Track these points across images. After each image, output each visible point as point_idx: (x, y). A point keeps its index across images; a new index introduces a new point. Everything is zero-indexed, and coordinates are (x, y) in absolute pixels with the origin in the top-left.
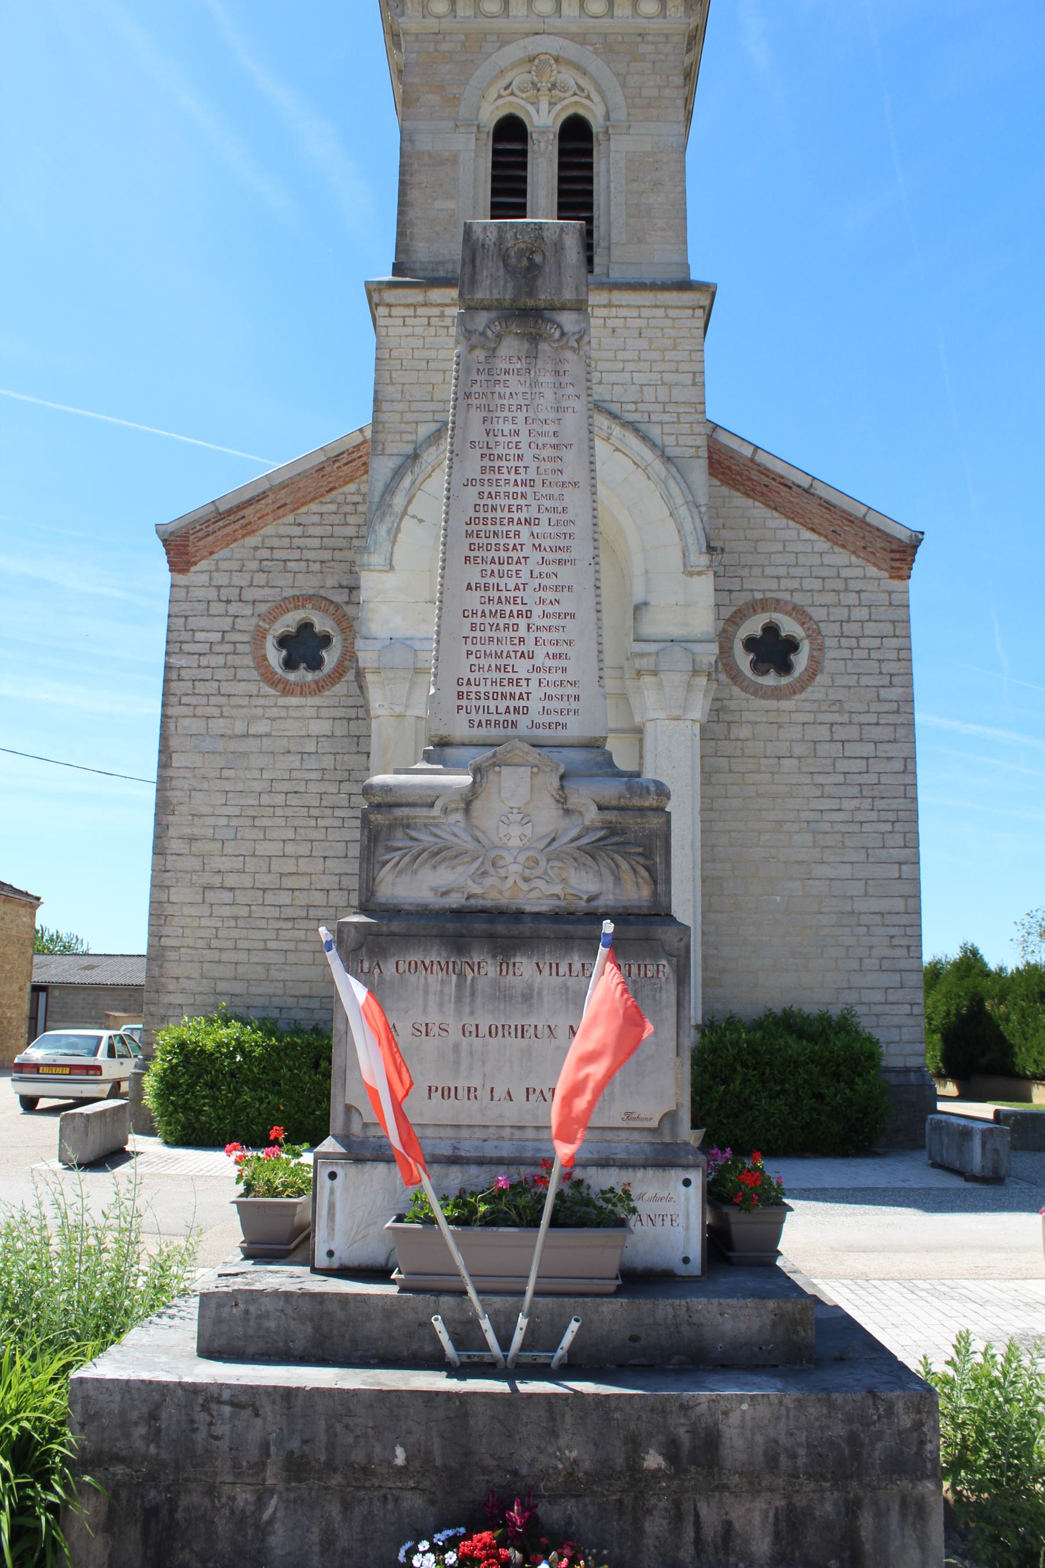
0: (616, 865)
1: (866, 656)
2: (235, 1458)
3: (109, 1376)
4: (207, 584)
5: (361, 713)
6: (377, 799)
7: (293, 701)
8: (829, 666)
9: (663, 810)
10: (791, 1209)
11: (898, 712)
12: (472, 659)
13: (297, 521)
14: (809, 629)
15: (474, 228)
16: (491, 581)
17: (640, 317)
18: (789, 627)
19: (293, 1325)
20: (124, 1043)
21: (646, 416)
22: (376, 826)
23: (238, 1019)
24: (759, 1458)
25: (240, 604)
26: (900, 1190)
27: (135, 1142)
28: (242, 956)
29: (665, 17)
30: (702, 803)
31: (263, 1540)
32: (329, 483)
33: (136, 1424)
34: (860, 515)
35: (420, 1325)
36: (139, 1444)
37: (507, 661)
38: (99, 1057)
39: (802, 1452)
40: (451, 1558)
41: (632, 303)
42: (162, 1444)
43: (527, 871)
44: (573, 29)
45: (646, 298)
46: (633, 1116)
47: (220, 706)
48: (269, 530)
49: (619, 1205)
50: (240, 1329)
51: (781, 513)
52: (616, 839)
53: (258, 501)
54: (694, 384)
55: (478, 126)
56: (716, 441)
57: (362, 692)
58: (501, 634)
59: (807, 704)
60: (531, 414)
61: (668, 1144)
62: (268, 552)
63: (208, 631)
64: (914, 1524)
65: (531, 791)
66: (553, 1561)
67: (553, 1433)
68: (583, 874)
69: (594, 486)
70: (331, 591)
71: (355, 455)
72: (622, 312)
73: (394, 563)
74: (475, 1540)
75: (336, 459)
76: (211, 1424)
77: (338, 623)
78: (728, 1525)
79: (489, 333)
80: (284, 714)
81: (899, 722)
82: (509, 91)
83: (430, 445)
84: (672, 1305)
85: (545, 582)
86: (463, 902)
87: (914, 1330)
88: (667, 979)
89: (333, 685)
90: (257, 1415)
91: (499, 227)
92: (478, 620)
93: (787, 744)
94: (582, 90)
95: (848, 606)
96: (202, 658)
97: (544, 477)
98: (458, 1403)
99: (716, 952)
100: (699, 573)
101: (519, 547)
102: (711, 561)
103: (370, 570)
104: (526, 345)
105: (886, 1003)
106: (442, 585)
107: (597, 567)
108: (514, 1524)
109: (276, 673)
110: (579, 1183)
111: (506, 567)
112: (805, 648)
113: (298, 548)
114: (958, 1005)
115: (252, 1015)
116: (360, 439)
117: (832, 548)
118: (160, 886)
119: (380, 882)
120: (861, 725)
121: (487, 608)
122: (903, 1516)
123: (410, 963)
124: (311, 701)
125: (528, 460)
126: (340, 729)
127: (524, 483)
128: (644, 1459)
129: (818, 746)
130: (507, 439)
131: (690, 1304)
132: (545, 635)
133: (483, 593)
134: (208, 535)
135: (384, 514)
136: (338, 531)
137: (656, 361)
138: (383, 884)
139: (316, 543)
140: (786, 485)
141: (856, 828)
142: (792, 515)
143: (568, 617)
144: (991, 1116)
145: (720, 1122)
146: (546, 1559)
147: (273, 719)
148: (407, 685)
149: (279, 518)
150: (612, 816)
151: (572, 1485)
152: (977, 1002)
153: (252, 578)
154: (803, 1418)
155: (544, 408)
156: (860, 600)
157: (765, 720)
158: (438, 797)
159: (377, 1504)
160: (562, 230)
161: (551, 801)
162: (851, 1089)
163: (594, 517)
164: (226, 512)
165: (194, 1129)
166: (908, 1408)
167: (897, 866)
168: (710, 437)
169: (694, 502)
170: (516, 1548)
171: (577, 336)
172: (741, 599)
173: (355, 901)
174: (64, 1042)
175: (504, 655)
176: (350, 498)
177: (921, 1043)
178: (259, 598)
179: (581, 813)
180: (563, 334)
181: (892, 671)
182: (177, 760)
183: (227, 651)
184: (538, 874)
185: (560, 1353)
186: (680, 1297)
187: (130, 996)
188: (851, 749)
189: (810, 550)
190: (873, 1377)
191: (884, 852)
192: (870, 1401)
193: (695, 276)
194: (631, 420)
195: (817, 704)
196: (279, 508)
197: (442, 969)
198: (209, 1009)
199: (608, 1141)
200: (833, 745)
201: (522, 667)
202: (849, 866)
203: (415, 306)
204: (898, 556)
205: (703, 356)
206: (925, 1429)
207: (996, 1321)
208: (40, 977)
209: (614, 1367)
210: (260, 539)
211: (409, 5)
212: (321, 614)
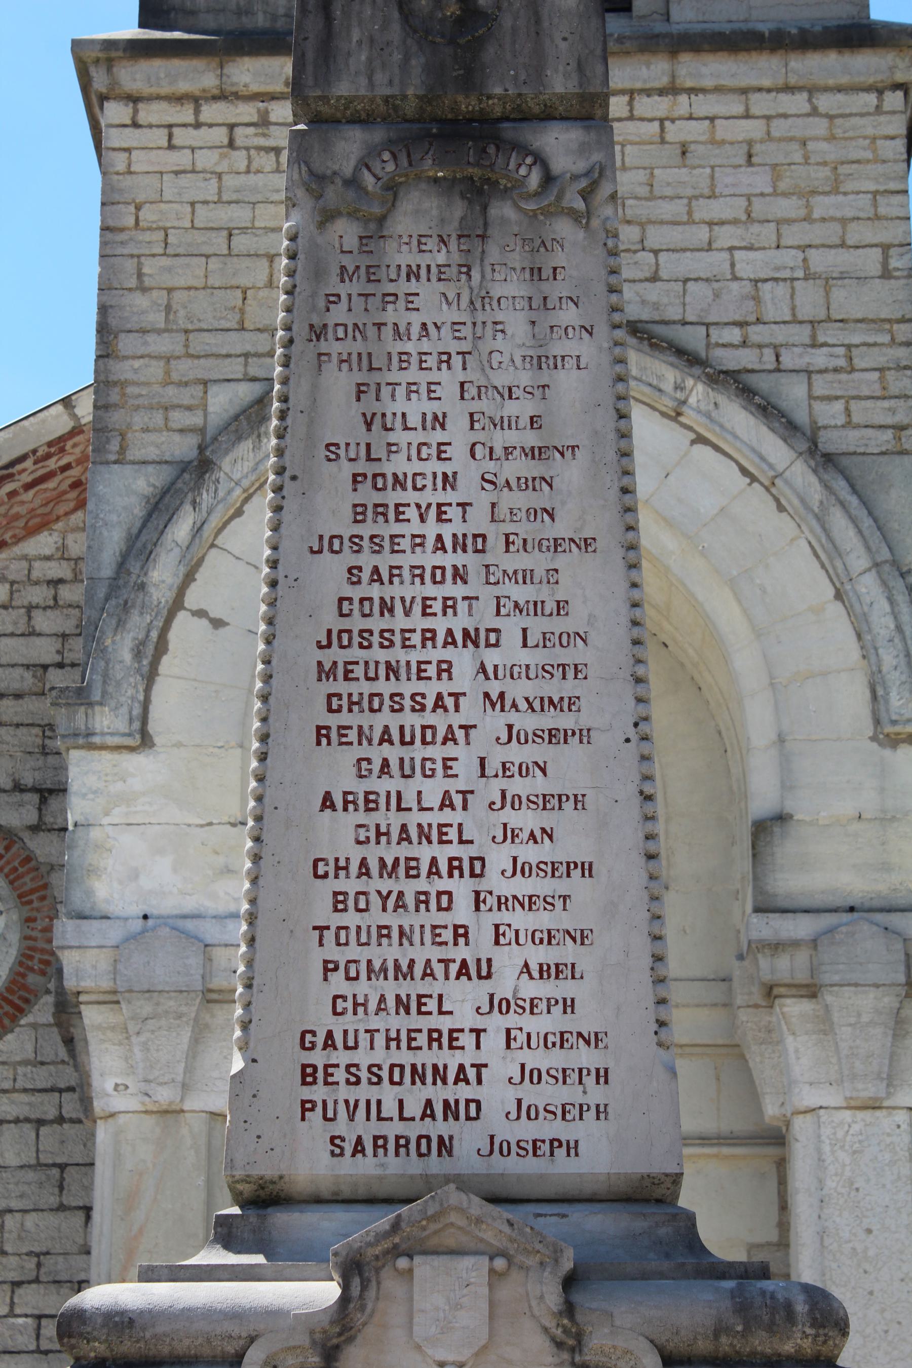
5: (70, 1108)
17: (747, 116)
37: (422, 987)
45: (762, 68)
58: (409, 919)
60: (473, 375)
65: (492, 1316)
72: (704, 105)
73: (151, 728)
79: (369, 180)
83: (239, 439)
85: (517, 786)
92: (351, 885)
97: (509, 528)
103: (92, 747)
104: (459, 209)
107: (646, 748)
111: (418, 752)
116: (64, 424)
127: (460, 544)
130: (416, 437)
132: (520, 919)
133: (361, 817)
135: (126, 607)
137: (789, 221)
148: (186, 1035)
155: (506, 359)
158: (252, 1340)
161: (539, 1344)
169: (895, 563)
171: (583, 183)
175: (418, 970)
176: (42, 570)
180: (548, 179)
194: (732, 366)
201: (464, 1001)
203: (196, 100)
205: (905, 206)
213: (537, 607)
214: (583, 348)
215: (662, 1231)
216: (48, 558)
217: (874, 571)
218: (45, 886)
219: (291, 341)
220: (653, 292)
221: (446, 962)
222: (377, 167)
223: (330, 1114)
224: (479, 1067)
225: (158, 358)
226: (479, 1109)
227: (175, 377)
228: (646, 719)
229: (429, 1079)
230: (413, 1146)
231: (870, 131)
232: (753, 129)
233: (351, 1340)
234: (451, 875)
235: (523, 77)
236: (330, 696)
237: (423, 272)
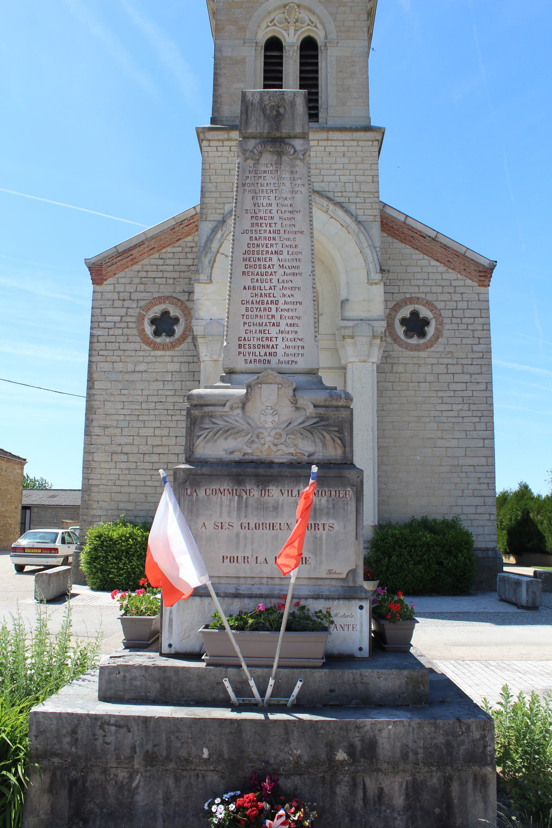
0: (323, 436)
1: (466, 328)
2: (118, 754)
3: (50, 711)
4: (112, 291)
5: (195, 359)
6: (195, 402)
7: (159, 353)
8: (446, 333)
9: (349, 407)
10: (418, 622)
11: (483, 358)
12: (246, 327)
14: (435, 313)
15: (247, 94)
16: (257, 284)
17: (344, 146)
18: (424, 312)
19: (149, 684)
20: (70, 536)
21: (347, 199)
22: (195, 417)
23: (131, 523)
24: (398, 754)
27: (75, 589)
28: (132, 490)
31: (133, 798)
33: (65, 736)
36: (66, 747)
38: (56, 543)
39: (421, 751)
40: (232, 807)
41: (339, 138)
42: (79, 747)
45: (347, 135)
46: (332, 572)
47: (120, 356)
48: (145, 262)
49: (325, 619)
51: (420, 251)
52: (323, 423)
53: (140, 246)
54: (373, 182)
55: (256, 43)
57: (196, 348)
58: (262, 313)
59: (434, 354)
60: (278, 195)
62: (145, 273)
63: (113, 316)
64: (480, 789)
65: (278, 397)
66: (287, 809)
67: (287, 741)
69: (312, 233)
70: (179, 294)
71: (191, 221)
72: (334, 143)
73: (212, 279)
74: (245, 798)
75: (181, 223)
76: (105, 736)
78: (381, 790)
79: (255, 151)
80: (154, 360)
81: (483, 363)
82: (273, 23)
85: (286, 285)
86: (241, 457)
87: (481, 686)
89: (180, 345)
90: (129, 731)
91: (261, 94)
92: (250, 306)
93: (423, 375)
94: (312, 23)
98: (236, 725)
99: (385, 486)
100: (376, 284)
103: (200, 283)
104: (275, 158)
106: (230, 287)
108: (266, 789)
109: (150, 338)
110: (303, 607)
111: (265, 277)
112: (433, 324)
113: (161, 271)
114: (516, 514)
115: (139, 520)
116: (194, 213)
119: (197, 446)
120: (463, 365)
121: (254, 299)
122: (475, 785)
124: (168, 353)
125: (276, 220)
126: (184, 368)
127: (274, 232)
128: (336, 755)
129: (440, 376)
130: (266, 208)
131: (362, 672)
132: (286, 314)
134: (113, 265)
136: (183, 262)
137: (352, 170)
139: (171, 268)
140: (422, 236)
141: (460, 420)
142: (426, 252)
144: (532, 574)
145: (388, 578)
146: (283, 808)
147: (148, 363)
149: (151, 255)
151: (298, 769)
152: (526, 513)
153: (137, 287)
154: (421, 733)
155: (285, 191)
157: (411, 362)
158: (228, 401)
159: (193, 778)
160: (295, 95)
161: (288, 403)
162: (457, 560)
163: (312, 250)
164: (122, 252)
165: (107, 581)
166: (478, 728)
168: (382, 211)
169: (373, 245)
170: (267, 802)
171: (303, 152)
172: (399, 297)
173: (182, 458)
174: (39, 535)
175: (264, 324)
177: (495, 535)
180: (295, 151)
181: (480, 336)
182: (97, 385)
185: (292, 698)
186: (356, 669)
187: (75, 511)
188: (457, 378)
189: (436, 271)
190: (460, 711)
191: (476, 432)
192: (458, 724)
193: (373, 123)
194: (339, 201)
195: (439, 354)
196: (150, 250)
198: (115, 518)
199: (319, 585)
200: (448, 375)
201: (274, 331)
203: (223, 141)
204: (483, 274)
206: (487, 739)
207: (531, 682)
208: (26, 501)
209: (321, 706)
210: (141, 266)
212: (173, 306)
213: (291, 246)
214: (302, 189)
215: (315, 380)
216: (190, 242)
220: (322, 185)
222: (257, 148)
224: (276, 345)
227: (218, 202)
231: (370, 150)
232: (345, 149)
233: (248, 401)
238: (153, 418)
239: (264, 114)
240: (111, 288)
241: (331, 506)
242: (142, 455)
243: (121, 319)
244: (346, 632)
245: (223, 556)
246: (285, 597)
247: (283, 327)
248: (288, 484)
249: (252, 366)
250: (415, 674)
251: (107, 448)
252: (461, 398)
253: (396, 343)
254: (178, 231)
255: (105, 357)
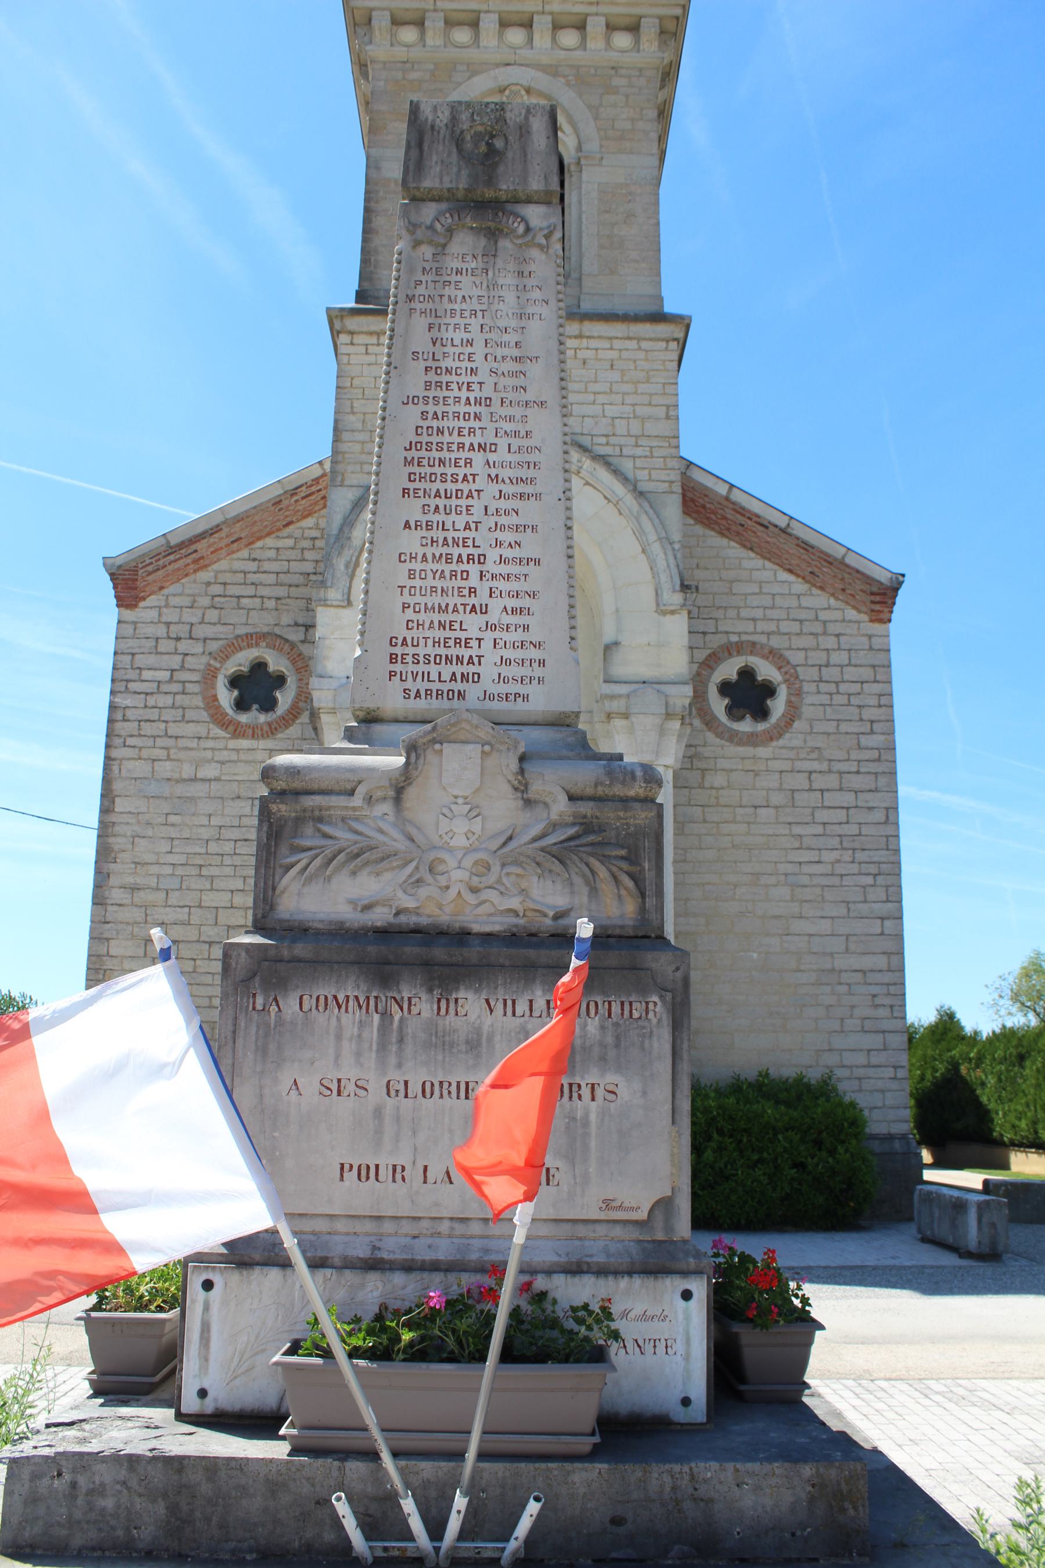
1: (846, 702)
4: (156, 620)
6: (281, 785)
7: (245, 743)
8: (807, 711)
9: (653, 801)
11: (879, 760)
12: (409, 614)
13: (252, 556)
14: (786, 673)
15: (422, 107)
16: (435, 518)
17: (611, 349)
18: (766, 671)
19: (139, 1504)
21: (617, 449)
22: (280, 819)
25: (191, 641)
26: (891, 1268)
29: (638, 51)
30: (675, 854)
32: (287, 517)
34: (839, 556)
35: (318, 1503)
43: (475, 879)
44: (545, 60)
45: (618, 329)
46: (614, 1204)
47: (167, 749)
50: (64, 1510)
51: (757, 553)
52: (591, 838)
53: (211, 534)
54: (668, 417)
56: (690, 479)
57: (316, 734)
58: (447, 584)
59: (784, 751)
60: (487, 321)
61: (660, 1242)
63: (156, 669)
65: (482, 774)
68: (549, 883)
70: (286, 629)
71: (314, 489)
72: (593, 343)
73: (352, 598)
77: (294, 662)
79: (438, 227)
80: (234, 756)
81: (880, 770)
84: (670, 1472)
85: (503, 520)
86: (391, 919)
88: (659, 1020)
89: (287, 728)
92: (417, 566)
93: (764, 793)
95: (827, 650)
96: (148, 697)
97: (504, 395)
100: (673, 612)
101: (470, 478)
102: (685, 599)
104: (483, 242)
105: (869, 1066)
106: (373, 523)
107: (568, 503)
109: (227, 714)
110: (542, 1296)
111: (454, 502)
112: (782, 693)
113: (253, 584)
117: (810, 590)
118: (100, 939)
119: (283, 892)
120: (840, 773)
123: (318, 998)
125: (483, 375)
127: (478, 402)
131: (695, 1470)
132: (502, 585)
133: (424, 533)
134: (158, 569)
136: (295, 566)
137: (628, 394)
138: (286, 895)
139: (271, 579)
140: (762, 525)
141: (836, 881)
142: (768, 556)
143: (532, 564)
144: (980, 1187)
147: (222, 763)
149: (233, 552)
150: (586, 808)
153: (204, 614)
155: (504, 314)
156: (839, 643)
157: (740, 767)
158: (360, 782)
160: (528, 111)
161: (506, 788)
162: (834, 1158)
167: (879, 921)
168: (684, 474)
169: (668, 539)
171: (546, 232)
172: (716, 642)
177: (906, 1108)
178: (211, 636)
179: (546, 805)
180: (528, 229)
181: (873, 718)
182: (120, 805)
183: (175, 690)
184: (490, 883)
185: (512, 1545)
186: (680, 1460)
188: (830, 799)
189: (787, 592)
191: (866, 906)
193: (669, 308)
194: (602, 453)
195: (795, 752)
196: (233, 542)
197: (360, 1007)
199: (580, 1239)
200: (812, 794)
201: (473, 624)
202: (829, 921)
204: (878, 598)
205: (677, 389)
207: (1031, 1435)
209: (589, 1562)
210: (212, 574)
211: (377, 33)
213: (516, 434)
217: (658, 543)
218: (307, 666)
219: (397, 302)
221: (464, 605)
222: (443, 220)
223: (404, 678)
224: (479, 657)
225: (359, 442)
226: (479, 677)
227: (366, 450)
228: (570, 490)
229: (454, 662)
230: (445, 694)
231: (663, 358)
232: (614, 354)
233: (410, 784)
234: (468, 563)
235: (517, 181)
236: (410, 474)
237: (464, 271)
238: (229, 871)
239: (460, 150)
240: (153, 614)
241: (610, 1039)
242: (207, 946)
243: (172, 675)
244: (649, 1358)
245: (342, 1165)
246: (498, 1271)
247: (495, 615)
248: (505, 984)
249: (422, 704)
250: (833, 1473)
251: (136, 930)
252: (838, 839)
253: (710, 729)
254: (287, 507)
255: (137, 750)
